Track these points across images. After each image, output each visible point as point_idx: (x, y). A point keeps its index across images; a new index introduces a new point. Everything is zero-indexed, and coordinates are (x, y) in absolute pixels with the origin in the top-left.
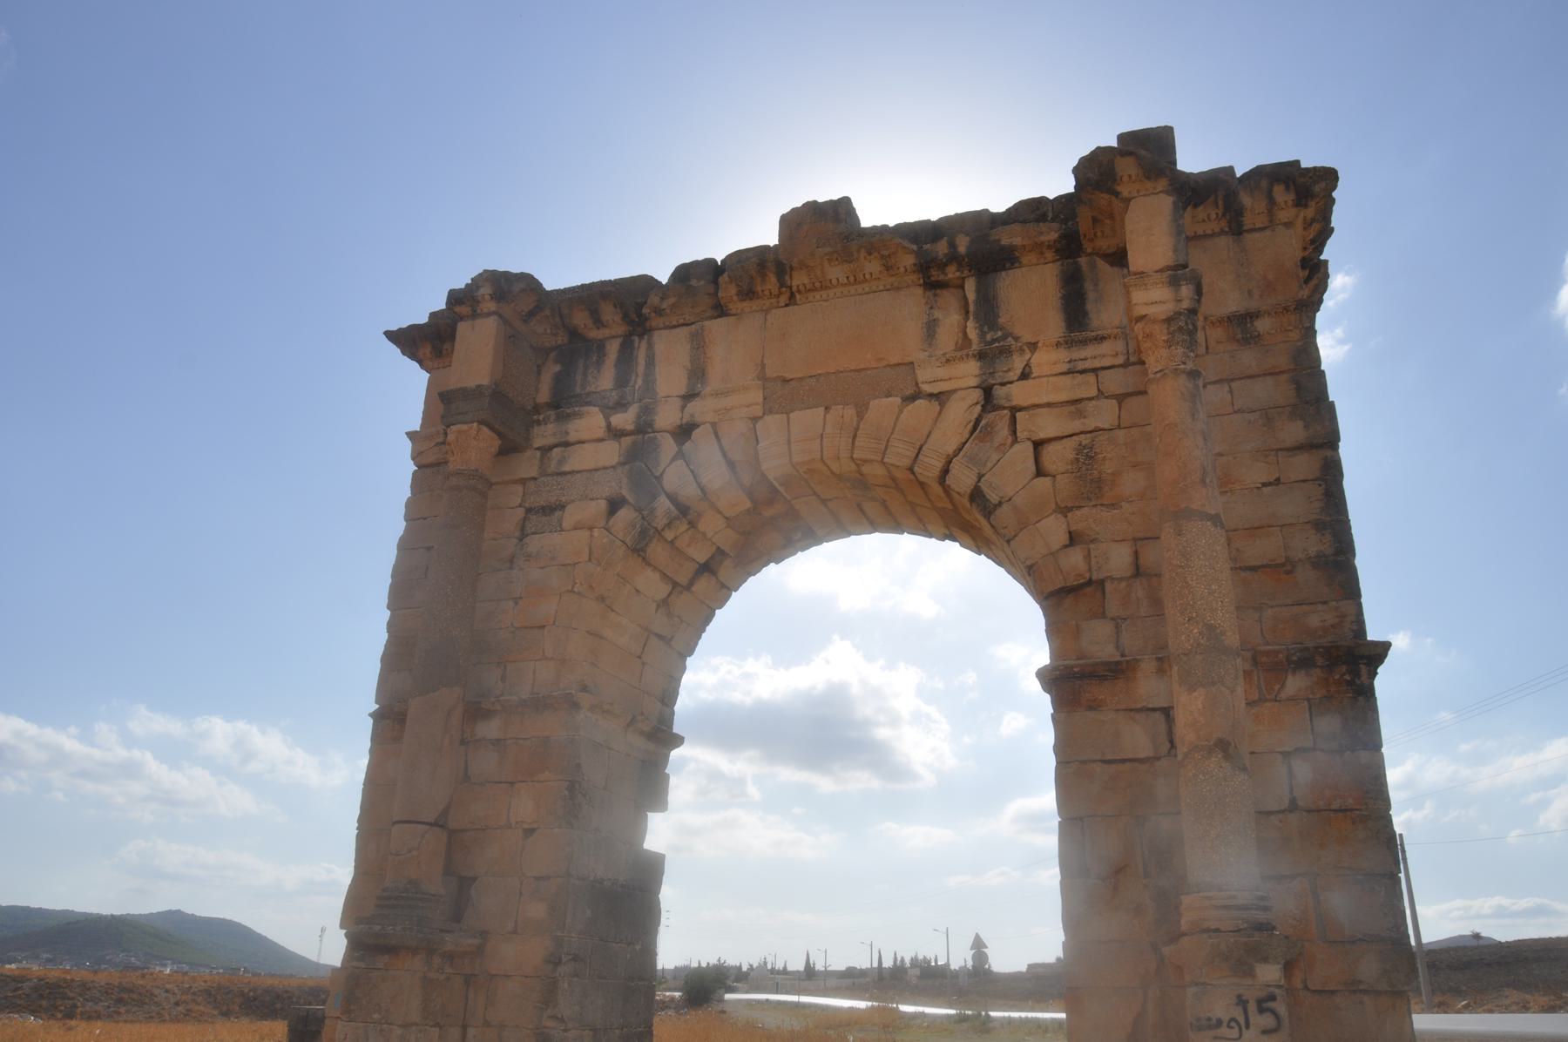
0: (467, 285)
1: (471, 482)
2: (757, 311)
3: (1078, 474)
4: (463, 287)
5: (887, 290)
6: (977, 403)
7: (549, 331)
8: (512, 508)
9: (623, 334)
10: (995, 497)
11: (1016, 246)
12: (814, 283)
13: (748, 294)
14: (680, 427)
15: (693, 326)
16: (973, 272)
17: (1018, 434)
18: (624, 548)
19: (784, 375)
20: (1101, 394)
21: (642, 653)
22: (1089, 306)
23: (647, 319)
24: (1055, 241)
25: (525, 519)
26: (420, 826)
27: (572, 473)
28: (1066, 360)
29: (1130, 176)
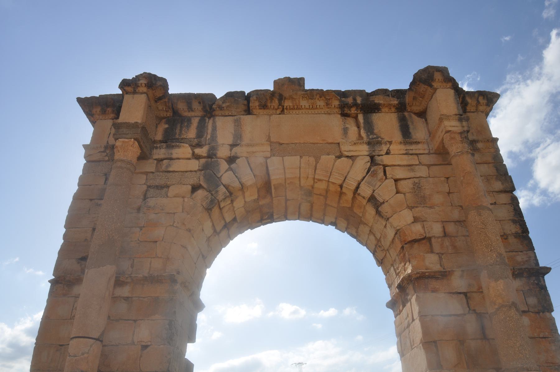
0: (133, 78)
1: (128, 166)
2: (266, 115)
3: (415, 194)
4: (131, 79)
5: (325, 114)
6: (368, 162)
7: (164, 109)
8: (140, 185)
9: (201, 116)
10: (382, 200)
11: (381, 104)
12: (294, 106)
13: (264, 106)
14: (230, 157)
15: (235, 117)
16: (362, 112)
17: (387, 176)
18: (202, 208)
19: (280, 141)
20: (420, 164)
21: (197, 262)
22: (411, 130)
23: (214, 110)
24: (397, 104)
25: (147, 191)
26: (90, 340)
27: (174, 172)
28: (405, 149)
29: (439, 79)
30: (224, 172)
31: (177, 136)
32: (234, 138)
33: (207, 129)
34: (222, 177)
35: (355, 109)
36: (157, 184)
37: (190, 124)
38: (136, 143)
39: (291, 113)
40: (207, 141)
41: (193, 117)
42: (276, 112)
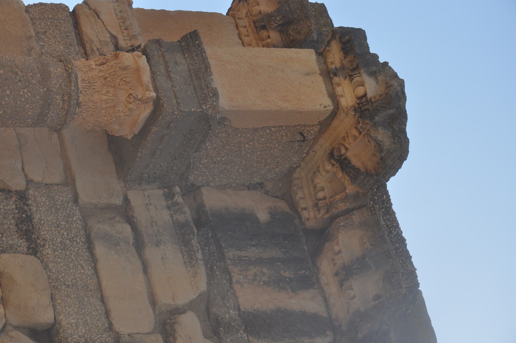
0: (375, 57)
4: (372, 51)
7: (321, 195)
8: (23, 169)
31: (231, 254)
36: (37, 217)
38: (147, 111)
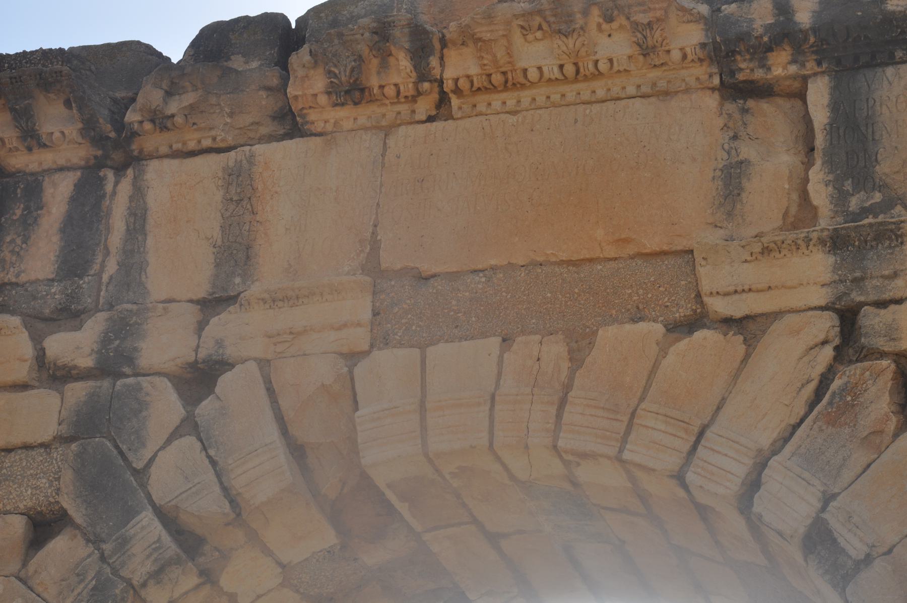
5: (643, 96)
6: (825, 342)
9: (83, 163)
12: (489, 75)
14: (193, 366)
16: (825, 65)
23: (134, 134)
30: (161, 442)
32: (217, 265)
33: (108, 229)
34: (153, 469)
35: (789, 58)
37: (36, 210)
39: (482, 108)
40: (104, 288)
41: (50, 171)
42: (413, 112)
